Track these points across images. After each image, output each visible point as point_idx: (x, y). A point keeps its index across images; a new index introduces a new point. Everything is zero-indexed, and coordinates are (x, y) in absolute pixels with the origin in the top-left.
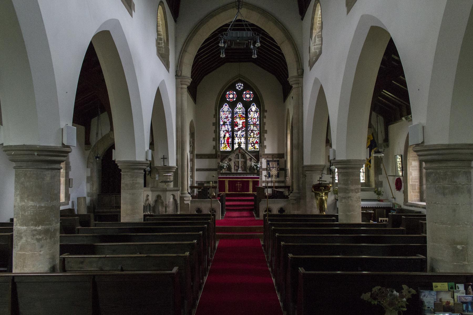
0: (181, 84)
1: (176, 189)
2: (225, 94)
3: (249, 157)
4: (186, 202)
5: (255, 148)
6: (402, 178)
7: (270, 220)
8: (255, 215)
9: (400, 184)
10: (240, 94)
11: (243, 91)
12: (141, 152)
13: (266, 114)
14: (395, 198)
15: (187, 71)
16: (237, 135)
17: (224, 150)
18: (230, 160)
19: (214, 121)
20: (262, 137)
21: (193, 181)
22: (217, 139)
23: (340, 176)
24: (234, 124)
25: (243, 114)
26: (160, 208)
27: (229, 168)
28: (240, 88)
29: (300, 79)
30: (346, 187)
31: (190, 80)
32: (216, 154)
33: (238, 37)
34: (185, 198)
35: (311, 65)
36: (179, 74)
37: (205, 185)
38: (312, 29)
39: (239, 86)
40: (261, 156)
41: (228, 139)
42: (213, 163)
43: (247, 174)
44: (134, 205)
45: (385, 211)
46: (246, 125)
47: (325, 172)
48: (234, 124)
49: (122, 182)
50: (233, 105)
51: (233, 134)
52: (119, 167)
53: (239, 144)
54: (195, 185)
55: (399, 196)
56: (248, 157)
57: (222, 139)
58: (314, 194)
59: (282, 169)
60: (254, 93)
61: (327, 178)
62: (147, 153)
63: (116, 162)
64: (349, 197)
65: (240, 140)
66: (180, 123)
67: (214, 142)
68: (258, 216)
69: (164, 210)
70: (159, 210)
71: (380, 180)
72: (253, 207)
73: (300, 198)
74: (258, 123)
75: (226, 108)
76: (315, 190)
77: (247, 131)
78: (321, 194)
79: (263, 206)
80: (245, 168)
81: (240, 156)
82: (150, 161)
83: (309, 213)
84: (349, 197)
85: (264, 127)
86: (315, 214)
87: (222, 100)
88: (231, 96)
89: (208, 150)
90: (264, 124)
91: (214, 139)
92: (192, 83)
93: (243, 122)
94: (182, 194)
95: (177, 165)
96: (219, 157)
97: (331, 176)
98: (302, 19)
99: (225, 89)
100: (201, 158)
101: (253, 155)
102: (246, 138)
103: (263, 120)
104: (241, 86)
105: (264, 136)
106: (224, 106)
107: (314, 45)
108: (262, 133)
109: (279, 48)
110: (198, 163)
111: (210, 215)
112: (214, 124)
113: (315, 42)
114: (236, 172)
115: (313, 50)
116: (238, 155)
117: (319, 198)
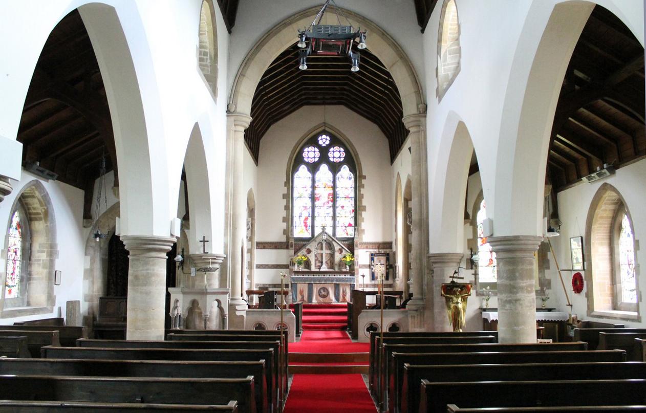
0: (235, 125)
1: (222, 290)
3: (339, 247)
4: (238, 313)
6: (583, 273)
7: (385, 341)
8: (350, 336)
9: (578, 283)
10: (324, 151)
11: (329, 146)
12: (164, 224)
13: (364, 181)
14: (571, 306)
15: (245, 106)
18: (309, 251)
19: (286, 192)
20: (358, 217)
21: (251, 284)
22: (289, 220)
23: (501, 264)
24: (313, 198)
26: (197, 322)
27: (307, 264)
29: (422, 119)
30: (512, 283)
31: (248, 120)
32: (287, 242)
33: (329, 35)
34: (237, 307)
35: (440, 95)
36: (232, 110)
37: (270, 289)
38: (440, 41)
39: (324, 140)
40: (357, 246)
41: (306, 219)
42: (282, 256)
43: (335, 273)
44: (148, 317)
45: (557, 326)
47: (463, 265)
49: (130, 271)
50: (313, 168)
52: (125, 248)
54: (255, 289)
55: (579, 300)
56: (337, 248)
58: (444, 299)
59: (391, 267)
60: (347, 151)
61: (466, 276)
62: (172, 224)
63: (121, 239)
64: (517, 300)
65: (323, 220)
66: (231, 186)
67: (285, 224)
68: (355, 336)
69: (203, 325)
70: (195, 325)
71: (547, 277)
72: (346, 324)
73: (425, 307)
75: (303, 171)
76: (446, 293)
78: (455, 299)
79: (363, 321)
80: (332, 264)
81: (324, 245)
82: (177, 237)
83: (438, 330)
84: (517, 300)
85: (361, 202)
86: (448, 331)
87: (297, 161)
88: (311, 154)
89: (276, 235)
90: (362, 196)
91: (285, 220)
92: (252, 123)
94: (232, 299)
95: (226, 253)
96: (292, 246)
97: (473, 271)
98: (423, 31)
99: (303, 142)
100: (264, 248)
101: (344, 244)
103: (360, 191)
105: (361, 215)
107: (444, 66)
108: (357, 210)
109: (388, 74)
110: (262, 256)
111: (279, 333)
112: (284, 196)
113: (445, 60)
114: (318, 270)
115: (442, 72)
116: (322, 244)
117: (452, 305)
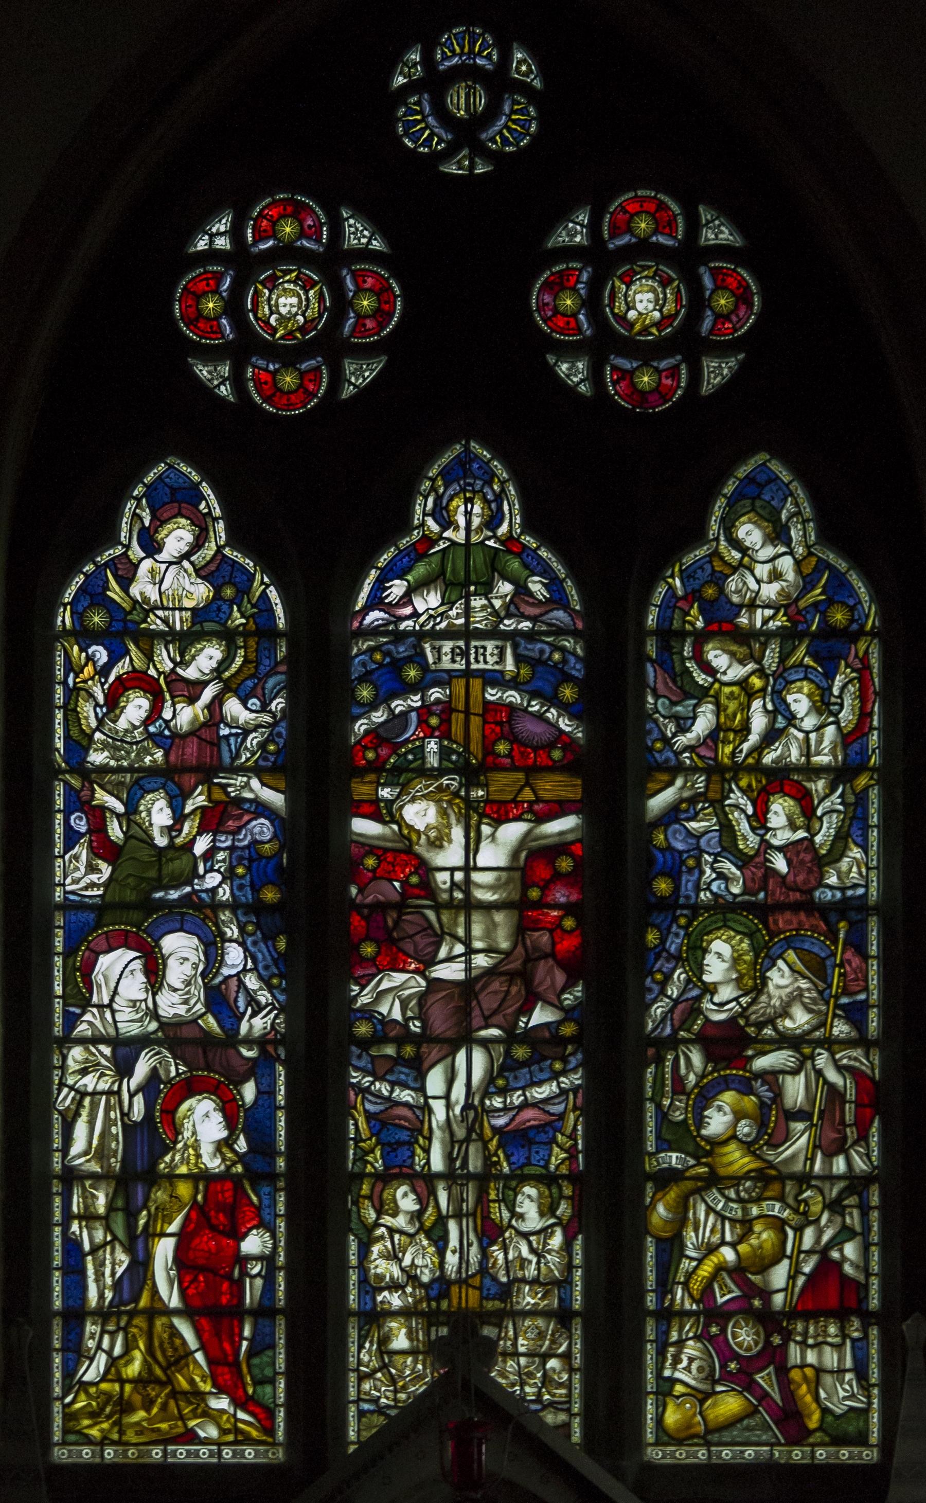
2: (154, 254)
5: (790, 1421)
10: (467, 267)
11: (531, 189)
16: (401, 1133)
17: (137, 1441)
24: (324, 908)
25: (541, 678)
28: (467, 133)
39: (465, 98)
46: (607, 912)
48: (324, 908)
50: (313, 509)
51: (319, 1104)
53: (461, 1326)
57: (84, 1219)
74: (854, 871)
77: (613, 1049)
88: (284, 297)
93: (532, 862)
102: (609, 1201)
104: (498, 83)
106: (134, 512)
